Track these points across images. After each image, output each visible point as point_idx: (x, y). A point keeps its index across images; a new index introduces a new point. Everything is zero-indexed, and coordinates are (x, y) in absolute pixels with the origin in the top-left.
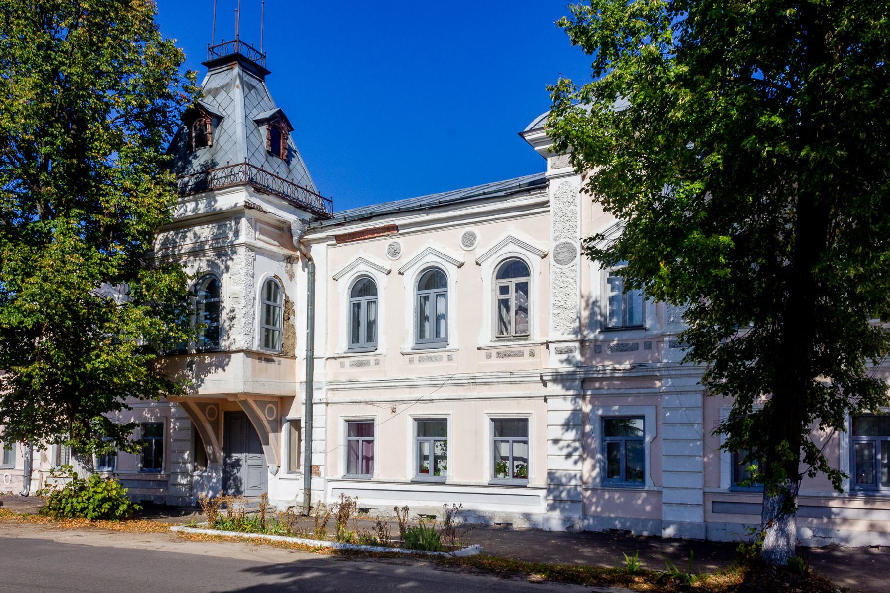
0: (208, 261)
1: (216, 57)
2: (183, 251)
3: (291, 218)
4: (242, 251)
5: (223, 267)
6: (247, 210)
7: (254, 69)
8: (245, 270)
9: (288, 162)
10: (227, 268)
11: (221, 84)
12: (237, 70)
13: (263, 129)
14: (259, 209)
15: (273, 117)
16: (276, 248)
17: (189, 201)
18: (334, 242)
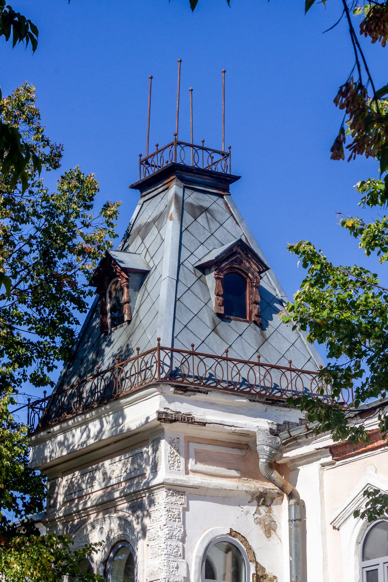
0: (120, 518)
1: (152, 171)
2: (89, 504)
3: (257, 424)
4: (161, 496)
5: (137, 527)
6: (166, 426)
7: (207, 179)
8: (166, 531)
9: (262, 325)
10: (144, 530)
11: (153, 216)
12: (175, 188)
13: (211, 279)
14: (189, 420)
15: (230, 253)
16: (231, 482)
17: (93, 420)
18: (330, 459)
